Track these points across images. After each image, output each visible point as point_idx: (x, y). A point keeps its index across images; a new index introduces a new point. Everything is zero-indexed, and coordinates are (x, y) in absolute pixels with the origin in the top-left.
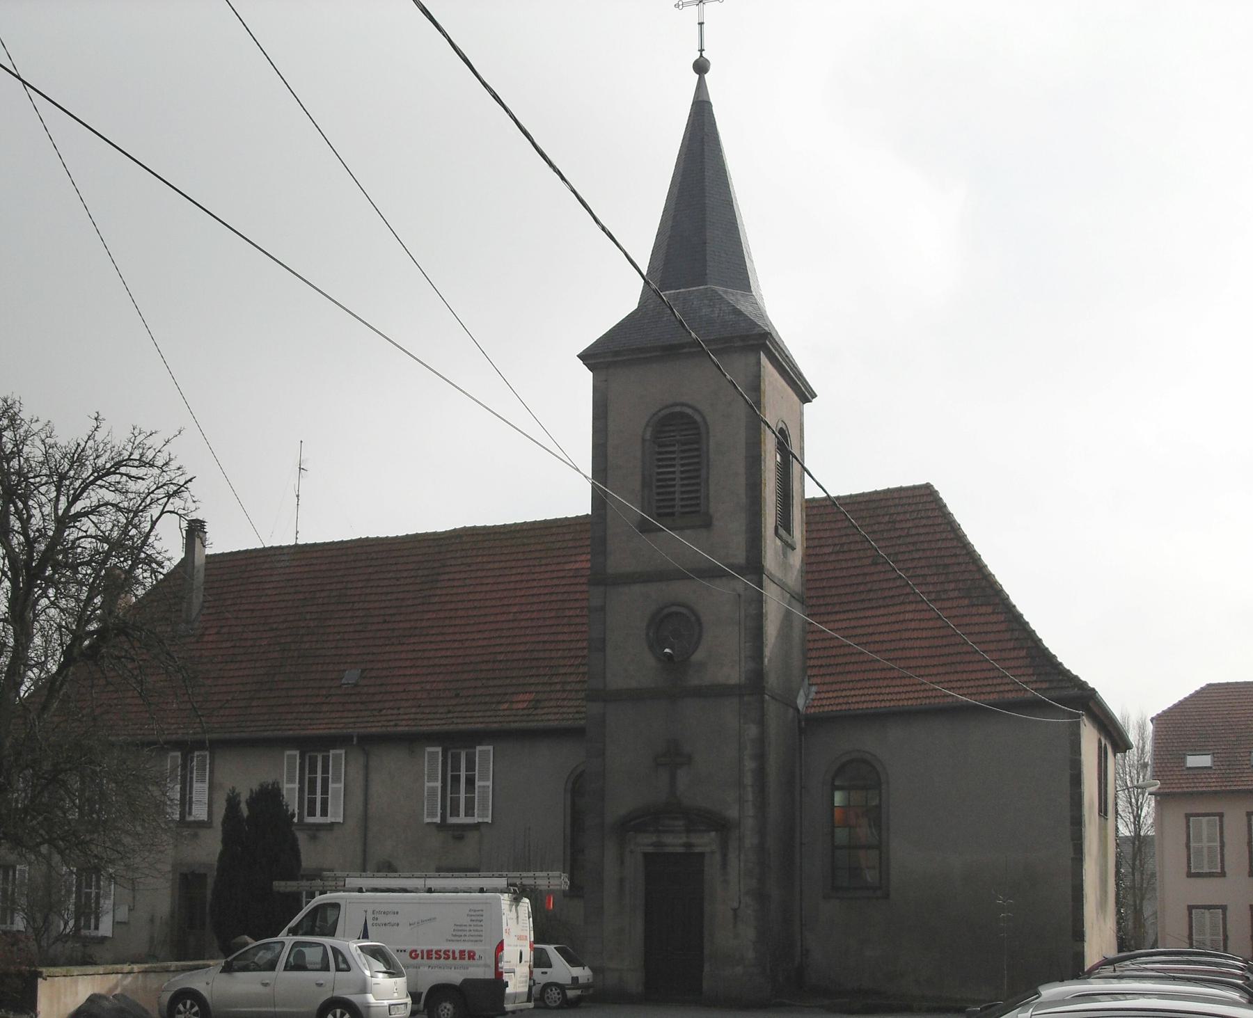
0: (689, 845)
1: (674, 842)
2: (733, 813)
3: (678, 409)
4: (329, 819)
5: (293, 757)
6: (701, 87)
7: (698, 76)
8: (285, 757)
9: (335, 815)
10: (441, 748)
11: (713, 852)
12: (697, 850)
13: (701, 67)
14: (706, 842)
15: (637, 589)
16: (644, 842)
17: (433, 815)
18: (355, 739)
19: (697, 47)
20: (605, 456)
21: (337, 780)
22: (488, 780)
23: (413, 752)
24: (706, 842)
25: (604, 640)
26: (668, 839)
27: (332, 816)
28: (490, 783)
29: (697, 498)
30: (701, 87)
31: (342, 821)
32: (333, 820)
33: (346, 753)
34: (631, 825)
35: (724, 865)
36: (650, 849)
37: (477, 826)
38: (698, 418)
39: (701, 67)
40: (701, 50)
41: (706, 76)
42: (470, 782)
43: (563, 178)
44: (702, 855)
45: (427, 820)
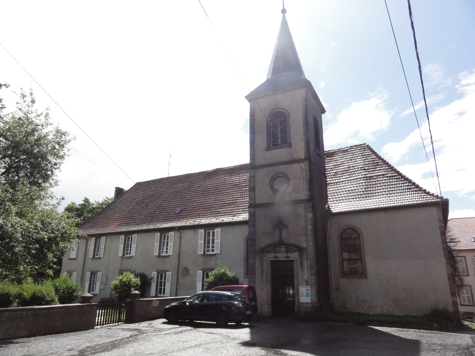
0: (288, 257)
1: (282, 256)
2: (304, 245)
3: (278, 110)
4: (215, 252)
5: (157, 236)
6: (284, 18)
7: (282, 15)
8: (156, 236)
9: (170, 253)
10: (159, 233)
11: (297, 260)
12: (291, 259)
13: (284, 11)
14: (294, 256)
15: (266, 169)
16: (270, 256)
17: (201, 251)
18: (176, 228)
19: (282, 6)
20: (254, 128)
21: (171, 242)
22: (172, 242)
23: (195, 232)
24: (294, 256)
25: (255, 187)
26: (279, 255)
27: (216, 251)
28: (219, 241)
29: (286, 136)
30: (284, 18)
31: (219, 253)
32: (216, 253)
33: (106, 238)
34: (264, 250)
35: (302, 264)
36: (273, 259)
37: (215, 255)
38: (285, 112)
39: (284, 11)
40: (284, 7)
41: (285, 14)
42: (213, 240)
43: (412, 23)
44: (293, 261)
45: (199, 253)
